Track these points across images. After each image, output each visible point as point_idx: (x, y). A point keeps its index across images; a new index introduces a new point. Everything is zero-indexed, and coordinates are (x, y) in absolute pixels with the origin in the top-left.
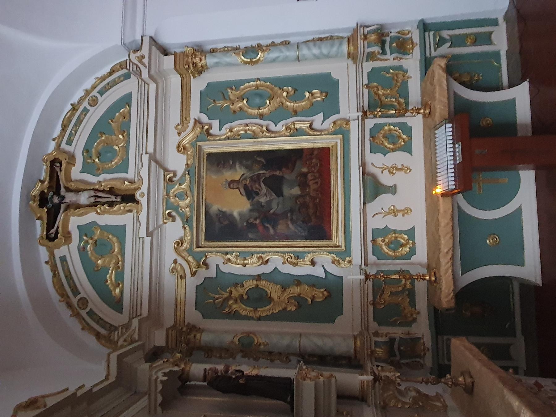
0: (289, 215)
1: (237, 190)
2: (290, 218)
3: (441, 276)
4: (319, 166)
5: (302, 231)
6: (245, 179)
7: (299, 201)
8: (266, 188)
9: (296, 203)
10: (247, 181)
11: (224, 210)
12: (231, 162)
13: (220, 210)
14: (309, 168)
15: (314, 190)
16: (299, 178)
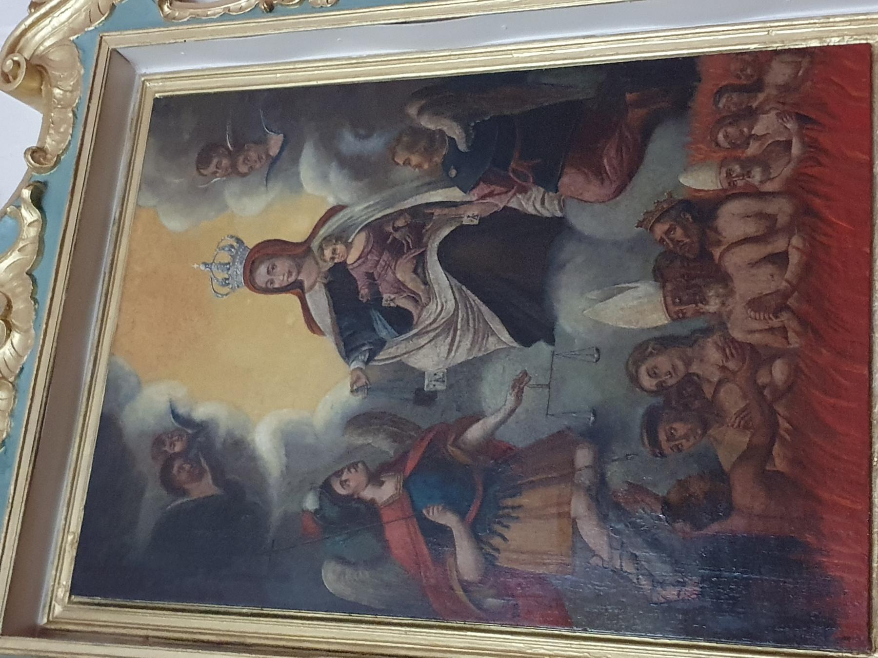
0: (583, 457)
1: (291, 300)
2: (585, 478)
3: (874, 452)
4: (801, 160)
5: (662, 569)
6: (341, 236)
7: (652, 374)
8: (455, 282)
9: (634, 379)
10: (349, 246)
11: (201, 412)
12: (275, 141)
13: (182, 410)
14: (729, 174)
15: (755, 304)
16: (660, 229)
